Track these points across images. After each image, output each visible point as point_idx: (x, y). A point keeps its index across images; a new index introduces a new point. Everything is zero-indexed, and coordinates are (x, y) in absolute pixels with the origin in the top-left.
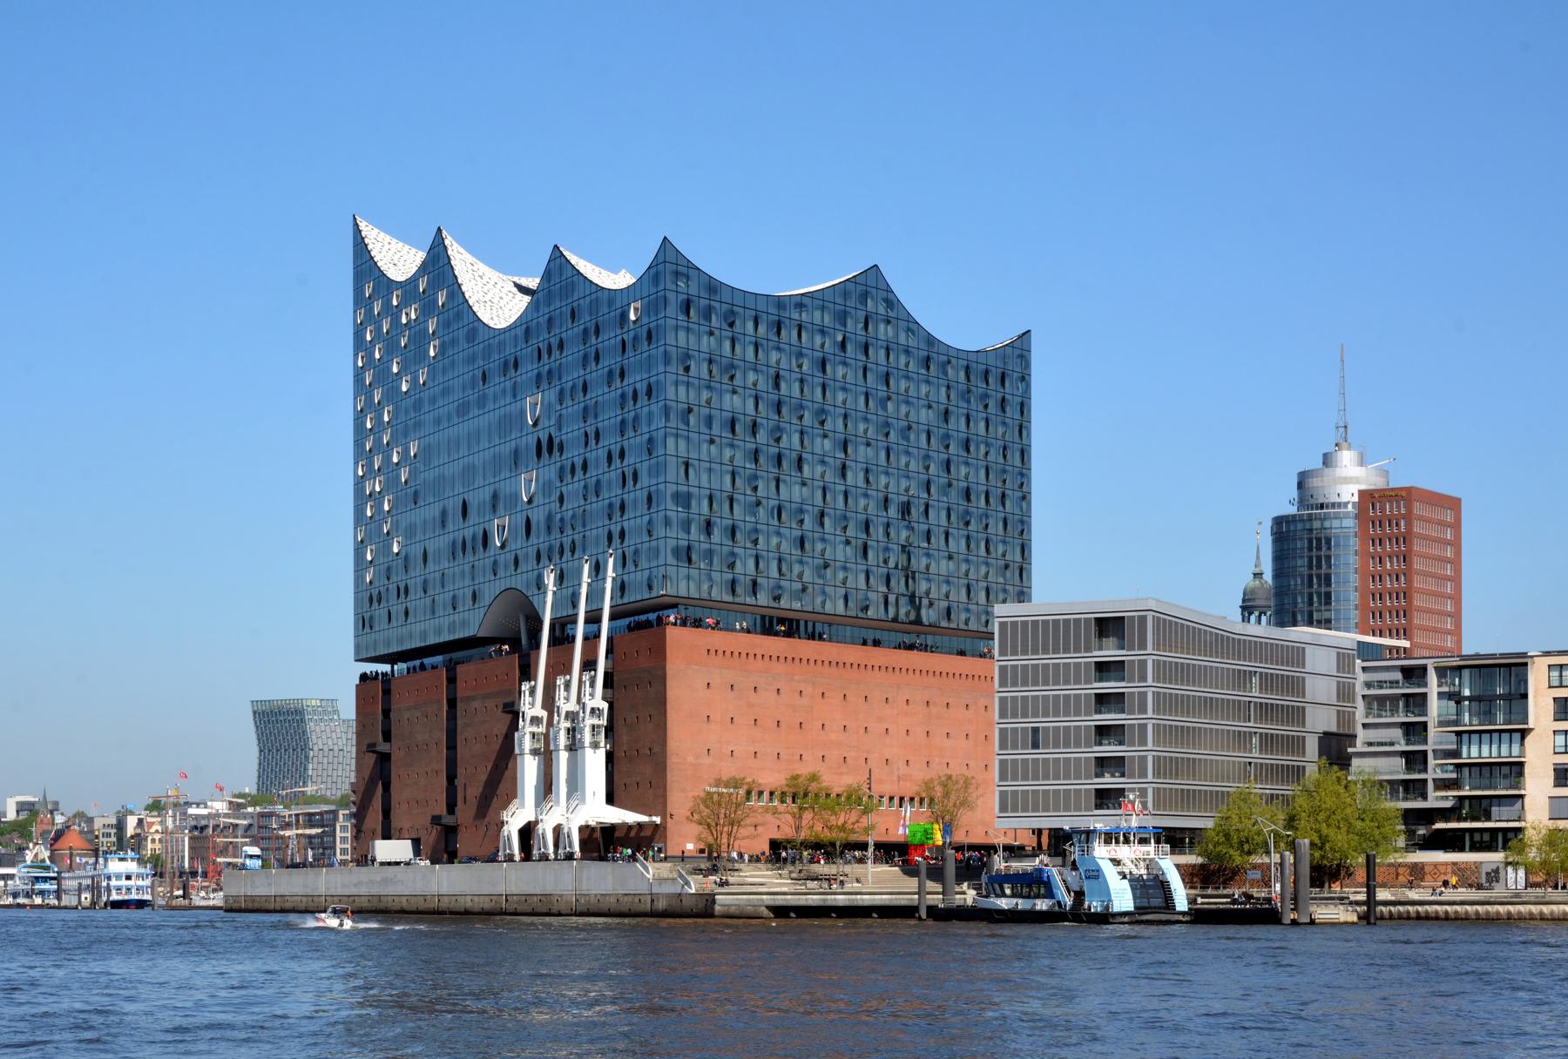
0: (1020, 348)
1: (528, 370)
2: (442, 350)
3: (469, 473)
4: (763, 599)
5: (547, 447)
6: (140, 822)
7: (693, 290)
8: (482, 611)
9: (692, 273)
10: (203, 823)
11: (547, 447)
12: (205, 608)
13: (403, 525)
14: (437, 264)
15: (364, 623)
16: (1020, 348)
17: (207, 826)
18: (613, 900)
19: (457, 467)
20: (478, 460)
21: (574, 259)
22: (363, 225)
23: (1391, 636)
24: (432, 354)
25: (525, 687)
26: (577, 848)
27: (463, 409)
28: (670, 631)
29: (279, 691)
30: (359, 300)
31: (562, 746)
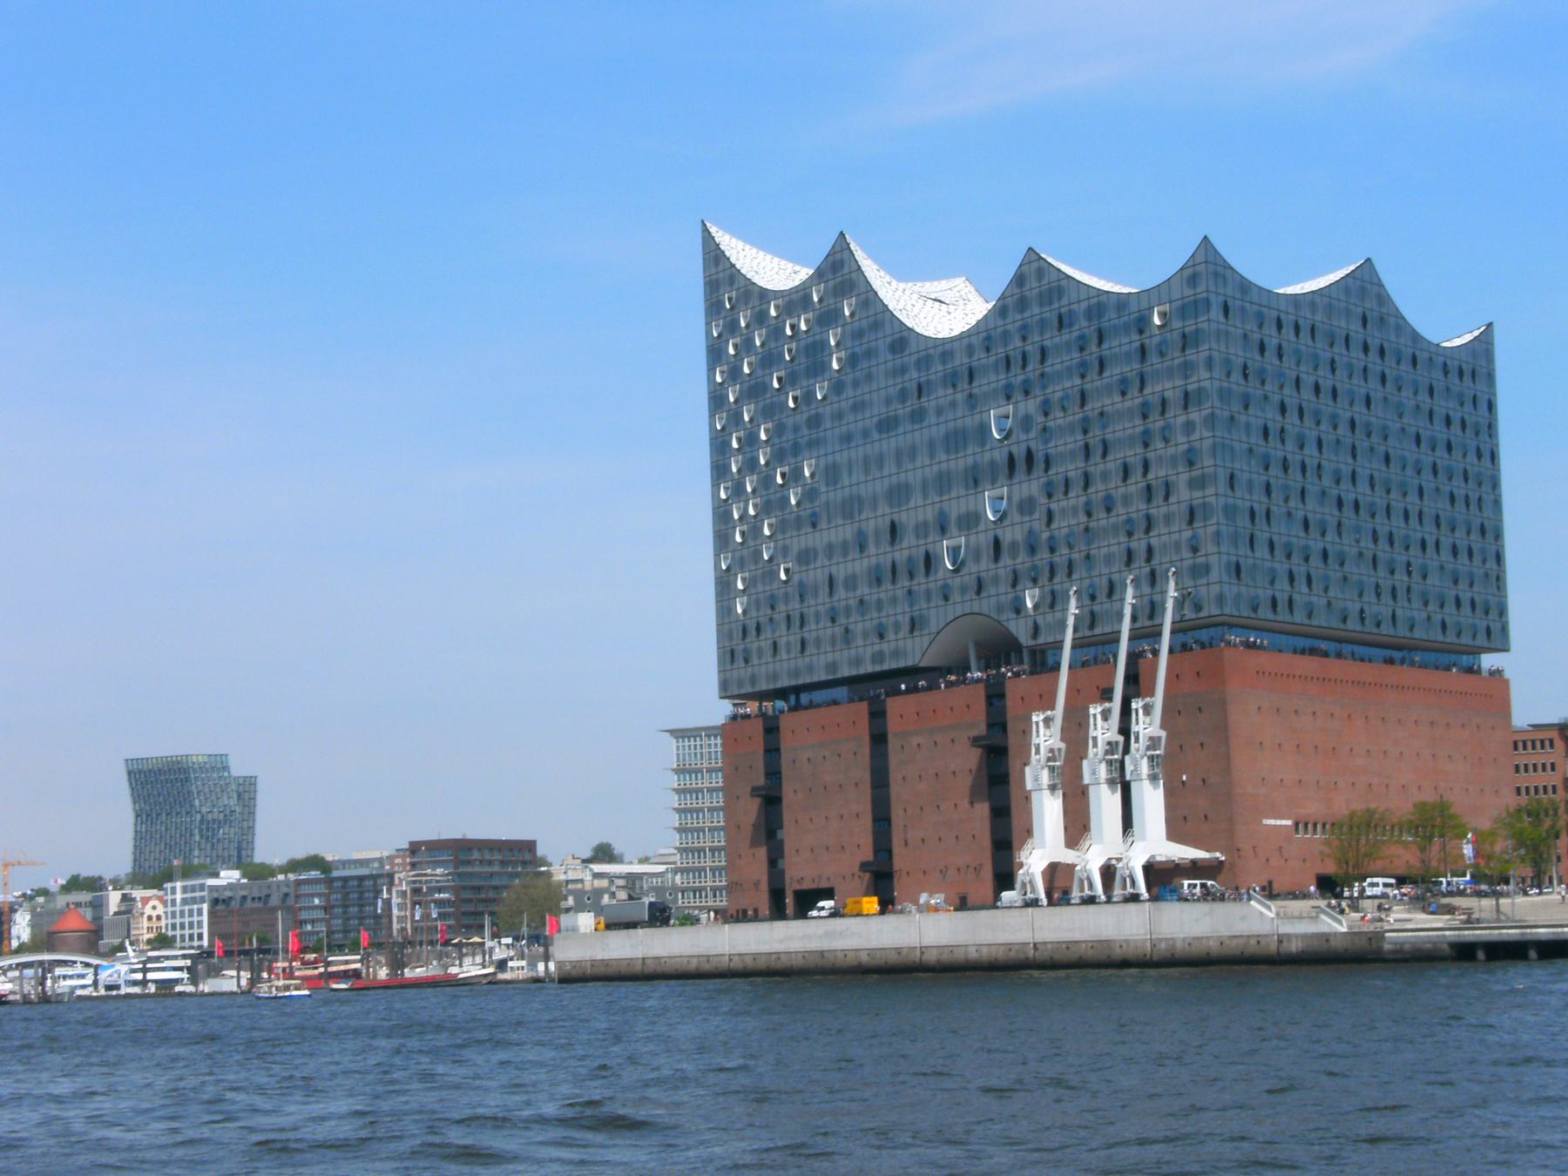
0: (1483, 346)
1: (990, 381)
2: (852, 361)
3: (898, 494)
4: (1299, 616)
5: (1017, 465)
6: (125, 898)
7: (1229, 292)
8: (926, 640)
9: (1229, 273)
10: (228, 894)
11: (1017, 465)
12: (534, 654)
13: (795, 550)
14: (839, 271)
15: (729, 656)
16: (1483, 346)
17: (231, 898)
18: (1253, 942)
19: (880, 487)
20: (915, 478)
21: (860, 255)
22: (713, 230)
23: (1159, 642)
24: (835, 366)
25: (1037, 717)
26: (1042, 896)
27: (887, 425)
28: (1228, 654)
29: (159, 746)
30: (713, 307)
31: (1045, 786)
